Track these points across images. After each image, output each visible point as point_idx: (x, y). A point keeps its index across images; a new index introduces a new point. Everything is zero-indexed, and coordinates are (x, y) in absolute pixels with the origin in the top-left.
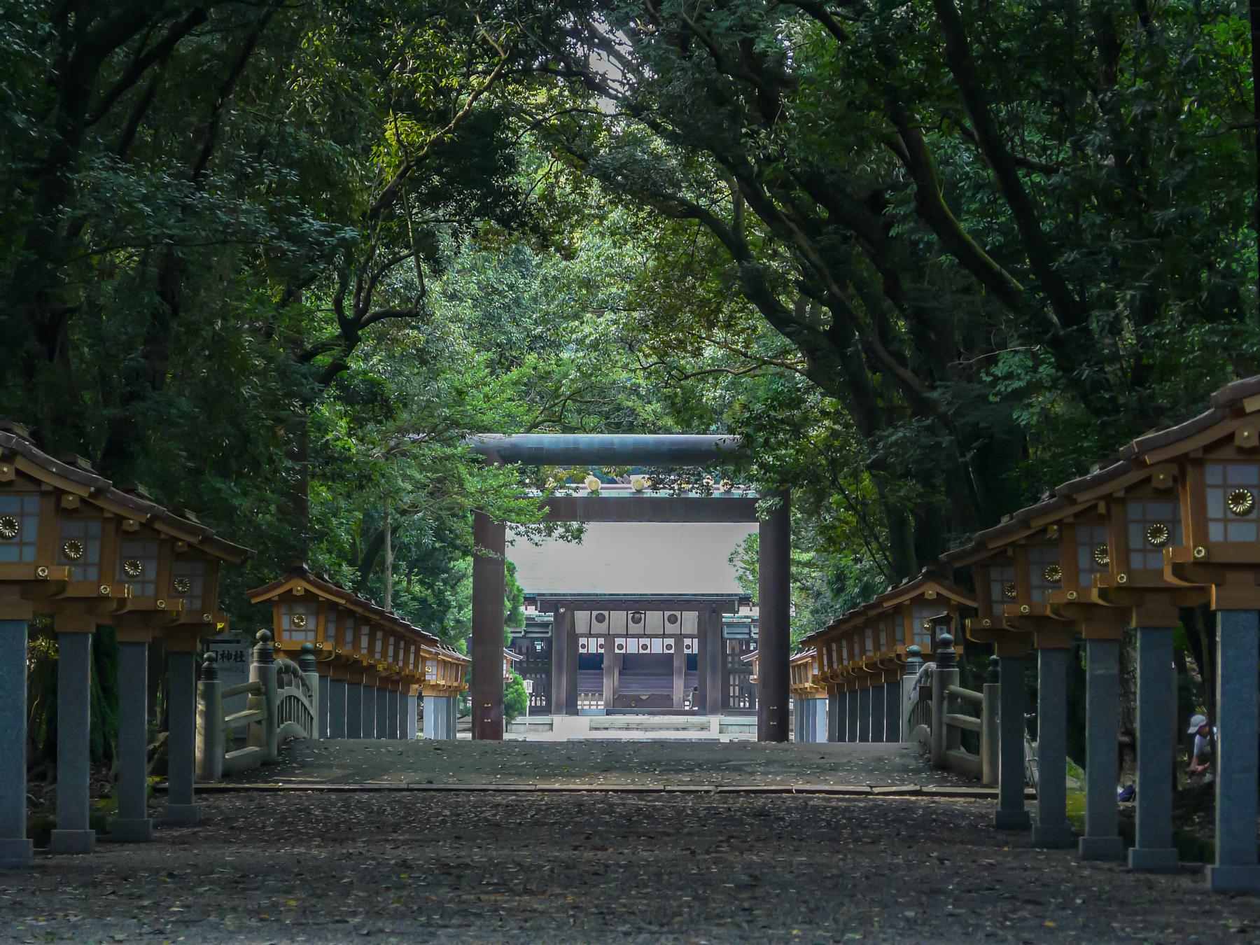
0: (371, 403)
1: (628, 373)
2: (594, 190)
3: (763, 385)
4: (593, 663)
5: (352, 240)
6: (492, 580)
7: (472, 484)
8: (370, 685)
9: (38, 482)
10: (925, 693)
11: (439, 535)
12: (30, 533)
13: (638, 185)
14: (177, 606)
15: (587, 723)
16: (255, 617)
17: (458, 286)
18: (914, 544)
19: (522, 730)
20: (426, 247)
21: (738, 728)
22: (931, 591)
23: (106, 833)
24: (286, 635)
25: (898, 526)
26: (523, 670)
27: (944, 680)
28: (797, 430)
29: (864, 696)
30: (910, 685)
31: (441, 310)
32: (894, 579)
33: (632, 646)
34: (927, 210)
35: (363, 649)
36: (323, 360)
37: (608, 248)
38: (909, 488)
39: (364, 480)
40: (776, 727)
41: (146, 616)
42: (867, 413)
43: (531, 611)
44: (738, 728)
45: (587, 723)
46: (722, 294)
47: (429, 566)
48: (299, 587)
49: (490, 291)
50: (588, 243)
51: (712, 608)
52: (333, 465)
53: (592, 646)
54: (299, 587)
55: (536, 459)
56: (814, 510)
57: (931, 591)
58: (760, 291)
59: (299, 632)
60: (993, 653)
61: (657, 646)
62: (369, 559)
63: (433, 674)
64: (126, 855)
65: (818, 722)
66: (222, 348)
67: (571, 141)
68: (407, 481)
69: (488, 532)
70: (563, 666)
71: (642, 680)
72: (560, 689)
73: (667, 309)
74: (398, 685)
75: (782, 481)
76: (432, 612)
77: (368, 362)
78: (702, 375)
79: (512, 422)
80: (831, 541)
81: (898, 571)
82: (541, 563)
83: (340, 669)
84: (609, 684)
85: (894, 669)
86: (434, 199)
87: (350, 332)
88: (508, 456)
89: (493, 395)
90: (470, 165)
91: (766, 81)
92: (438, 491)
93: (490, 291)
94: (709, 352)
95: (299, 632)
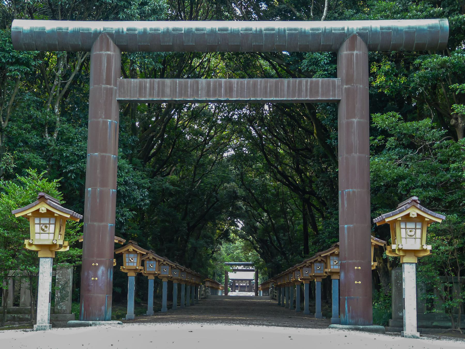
0: (215, 259)
1: (242, 255)
2: (238, 237)
3: (256, 258)
4: (237, 286)
5: (212, 243)
6: (227, 277)
7: (225, 268)
8: (215, 290)
9: (155, 259)
10: (271, 291)
11: (221, 272)
12: (154, 267)
13: (242, 237)
14: (197, 282)
15: (237, 293)
16: (204, 283)
17: (223, 248)
18: (271, 275)
19: (230, 294)
20: (221, 244)
21: (252, 294)
22: (272, 280)
23: (192, 305)
24: (127, 264)
25: (269, 273)
26: (230, 287)
27: (273, 290)
28: (259, 263)
29: (265, 290)
30: (270, 290)
31: (222, 249)
32: (269, 279)
33: (241, 284)
34: (271, 242)
35: (214, 286)
36: (210, 255)
37: (239, 243)
38: (271, 269)
39: (214, 268)
40: (257, 294)
41: (195, 283)
42: (266, 261)
43: (230, 281)
44: (252, 294)
45: (237, 293)
46: (251, 248)
47: (220, 276)
48: (208, 279)
49: (227, 247)
50: (237, 243)
51: (250, 280)
52: (210, 266)
53: (237, 284)
54: (208, 279)
55: (231, 265)
56: (261, 271)
57: (272, 280)
58: (255, 248)
59: (208, 284)
60: (278, 288)
61: (244, 285)
62: (214, 275)
63: (220, 288)
64: (193, 307)
65: (261, 293)
66: (200, 255)
67: (235, 232)
68: (218, 267)
69: (226, 273)
70: (234, 288)
71: (242, 289)
72: (234, 289)
73: (246, 249)
74: (217, 289)
75: (257, 268)
76: (220, 281)
77: (215, 255)
78: (249, 256)
79: (229, 261)
80: (262, 274)
81: (269, 278)
82: (232, 276)
83: (212, 288)
84: (239, 289)
85: (268, 288)
86: (221, 239)
87: (213, 253)
88: (229, 264)
89: (227, 258)
90: (225, 235)
91: (256, 228)
92: (221, 268)
93: (227, 247)
94: (250, 254)
95: (208, 284)
